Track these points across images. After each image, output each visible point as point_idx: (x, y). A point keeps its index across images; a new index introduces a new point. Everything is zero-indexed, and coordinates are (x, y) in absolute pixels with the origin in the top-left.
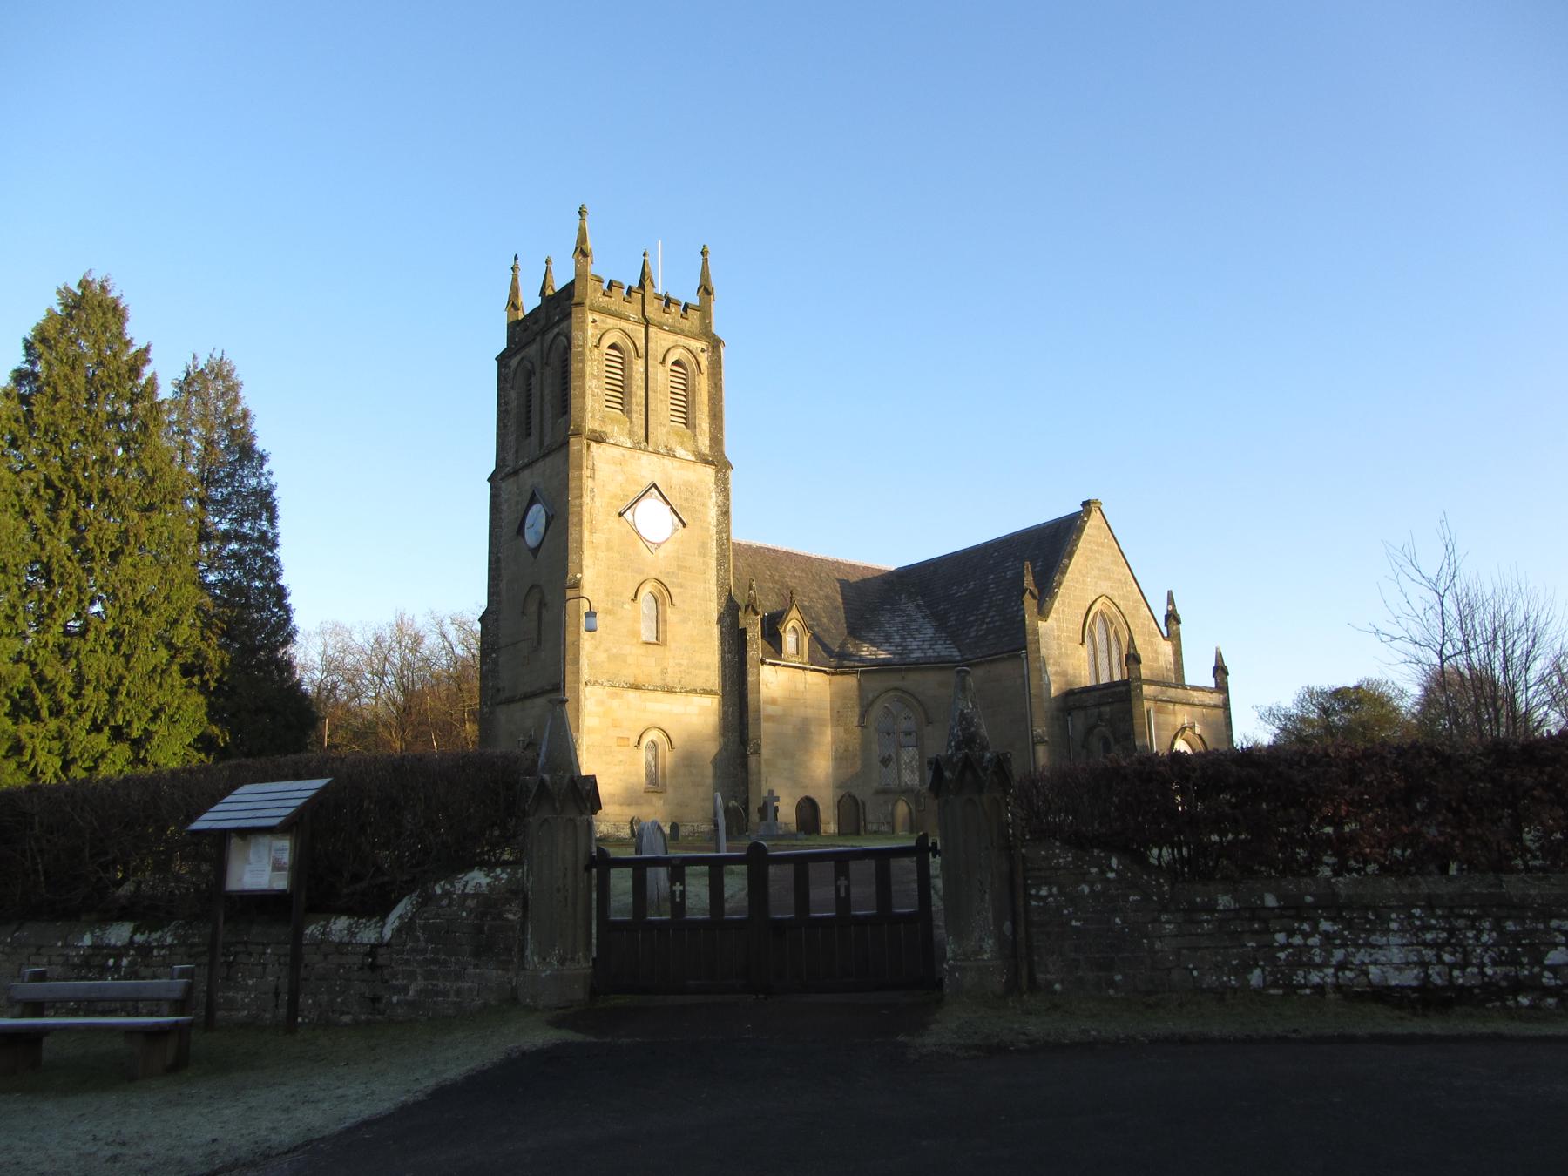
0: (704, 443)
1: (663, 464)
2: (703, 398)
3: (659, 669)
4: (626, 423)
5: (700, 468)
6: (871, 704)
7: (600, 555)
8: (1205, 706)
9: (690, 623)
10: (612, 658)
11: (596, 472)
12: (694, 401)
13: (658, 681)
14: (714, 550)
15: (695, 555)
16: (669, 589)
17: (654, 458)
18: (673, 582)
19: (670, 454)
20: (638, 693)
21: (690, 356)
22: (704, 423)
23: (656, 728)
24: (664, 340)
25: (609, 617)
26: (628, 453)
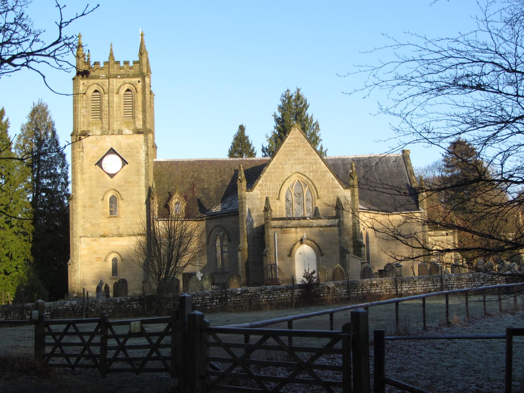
0: (139, 125)
1: (117, 138)
2: (139, 103)
3: (116, 227)
4: (99, 124)
5: (136, 136)
6: (210, 234)
7: (86, 183)
8: (321, 227)
9: (131, 206)
10: (92, 225)
11: (84, 149)
12: (134, 106)
13: (115, 232)
14: (144, 171)
15: (133, 176)
16: (120, 192)
17: (112, 136)
18: (123, 189)
19: (120, 133)
20: (106, 239)
21: (132, 86)
22: (140, 115)
23: (113, 252)
24: (119, 82)
25: (91, 209)
26: (99, 137)
